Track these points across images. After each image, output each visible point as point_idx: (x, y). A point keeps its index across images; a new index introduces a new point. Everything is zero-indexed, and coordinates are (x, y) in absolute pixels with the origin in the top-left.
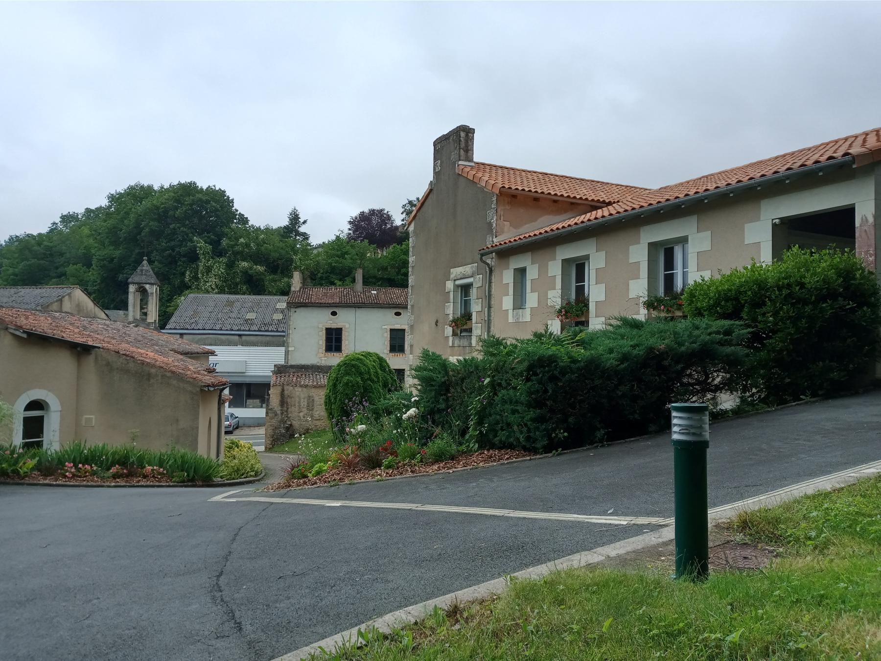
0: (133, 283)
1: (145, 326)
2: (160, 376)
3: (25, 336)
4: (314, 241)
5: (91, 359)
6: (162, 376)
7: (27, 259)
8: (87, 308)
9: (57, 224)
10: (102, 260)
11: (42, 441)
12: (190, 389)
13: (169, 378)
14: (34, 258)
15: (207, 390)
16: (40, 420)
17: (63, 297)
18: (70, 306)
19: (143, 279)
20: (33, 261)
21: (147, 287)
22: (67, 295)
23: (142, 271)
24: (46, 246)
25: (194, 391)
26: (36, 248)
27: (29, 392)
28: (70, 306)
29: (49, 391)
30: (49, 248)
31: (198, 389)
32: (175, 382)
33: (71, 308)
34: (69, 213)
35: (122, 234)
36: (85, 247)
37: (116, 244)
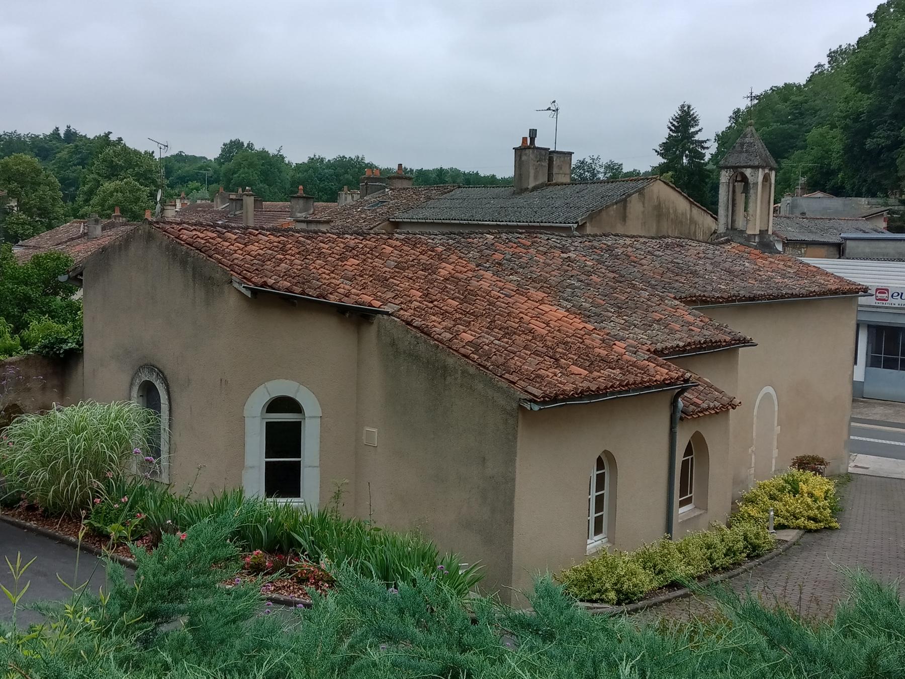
0: (727, 168)
1: (742, 240)
2: (460, 372)
3: (248, 294)
4: (111, 139)
5: (371, 333)
6: (463, 373)
7: (767, 125)
8: (675, 211)
9: (822, 66)
10: (845, 118)
11: (898, 369)
12: (503, 403)
13: (473, 376)
14: (777, 122)
15: (529, 409)
16: (295, 429)
17: (630, 195)
18: (642, 209)
19: (742, 159)
20: (775, 126)
21: (748, 172)
22: (636, 192)
23: (742, 145)
24: (794, 102)
25: (509, 408)
26: (780, 106)
27: (269, 385)
28: (642, 209)
29: (302, 384)
30: (796, 105)
31: (515, 405)
32: (480, 386)
33: (643, 212)
34: (840, 46)
35: (875, 73)
36: (846, 98)
37: (865, 89)
